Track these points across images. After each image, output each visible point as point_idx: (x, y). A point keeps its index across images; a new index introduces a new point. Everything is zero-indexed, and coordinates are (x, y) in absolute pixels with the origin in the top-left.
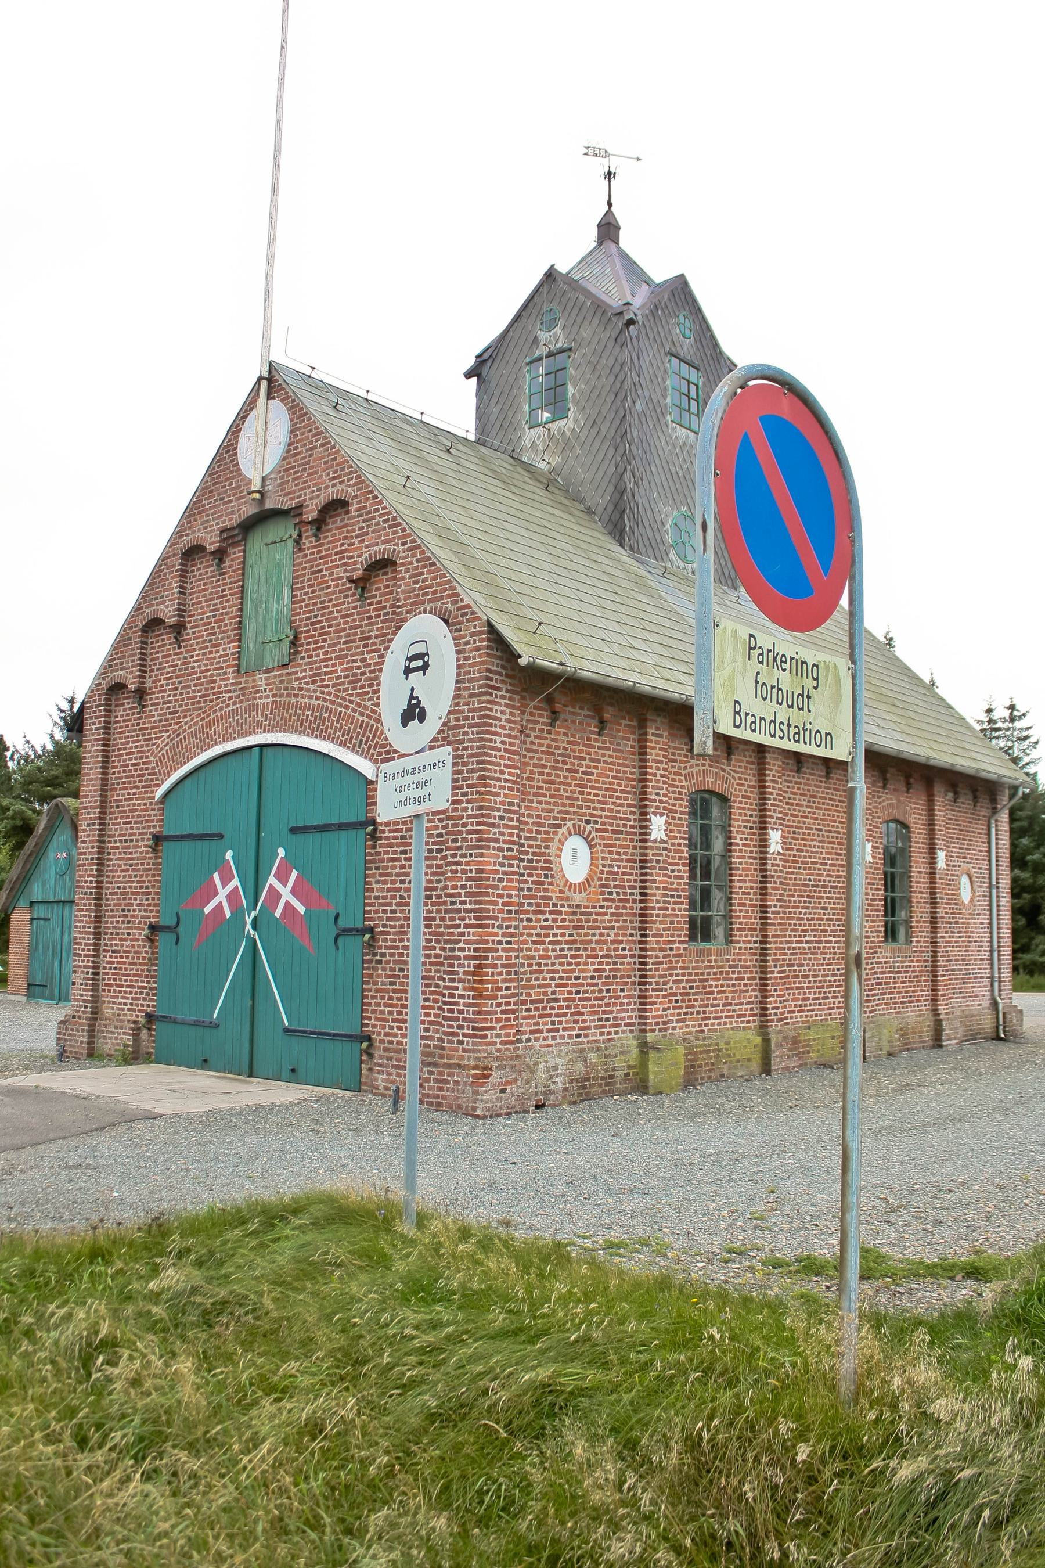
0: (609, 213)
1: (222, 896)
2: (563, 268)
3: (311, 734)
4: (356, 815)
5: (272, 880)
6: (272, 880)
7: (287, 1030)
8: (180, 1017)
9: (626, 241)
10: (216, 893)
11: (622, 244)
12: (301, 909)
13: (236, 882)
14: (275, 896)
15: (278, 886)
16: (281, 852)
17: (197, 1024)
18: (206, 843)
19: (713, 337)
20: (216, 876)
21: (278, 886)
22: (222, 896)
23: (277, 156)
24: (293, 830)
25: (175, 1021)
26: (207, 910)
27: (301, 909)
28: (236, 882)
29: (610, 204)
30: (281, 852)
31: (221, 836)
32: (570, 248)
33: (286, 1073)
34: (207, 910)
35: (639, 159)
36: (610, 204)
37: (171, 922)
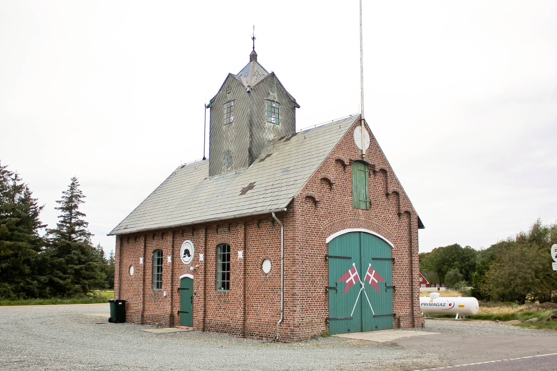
0: (254, 50)
1: (352, 277)
2: (235, 72)
3: (357, 227)
4: (389, 257)
5: (368, 273)
6: (368, 273)
7: (374, 316)
8: (339, 317)
9: (259, 60)
10: (350, 276)
11: (258, 61)
12: (377, 281)
13: (356, 273)
14: (369, 278)
15: (369, 274)
16: (370, 265)
17: (346, 319)
18: (345, 260)
19: (380, 151)
20: (350, 271)
21: (369, 274)
22: (352, 277)
23: (362, 78)
24: (373, 259)
25: (337, 319)
26: (347, 281)
27: (377, 281)
28: (356, 273)
29: (254, 48)
30: (370, 265)
31: (351, 258)
32: (237, 64)
33: (374, 328)
34: (347, 281)
35: (254, 38)
36: (254, 48)
37: (335, 286)
